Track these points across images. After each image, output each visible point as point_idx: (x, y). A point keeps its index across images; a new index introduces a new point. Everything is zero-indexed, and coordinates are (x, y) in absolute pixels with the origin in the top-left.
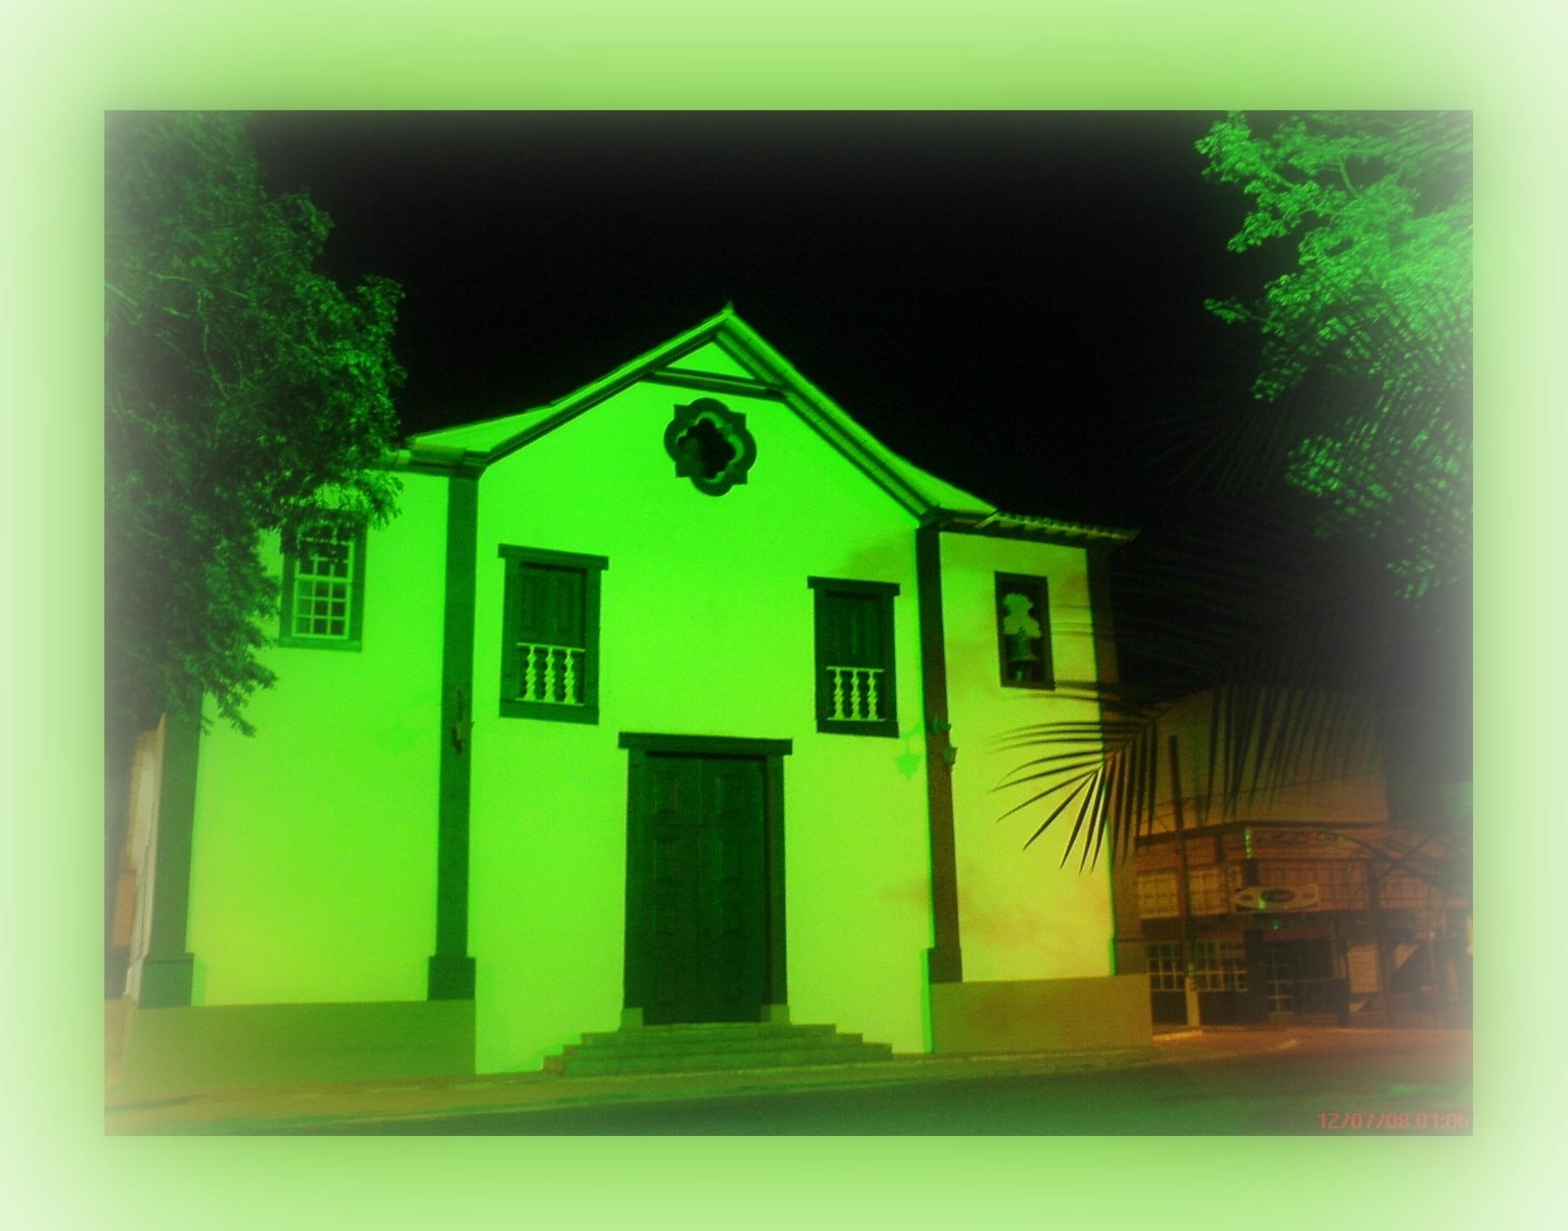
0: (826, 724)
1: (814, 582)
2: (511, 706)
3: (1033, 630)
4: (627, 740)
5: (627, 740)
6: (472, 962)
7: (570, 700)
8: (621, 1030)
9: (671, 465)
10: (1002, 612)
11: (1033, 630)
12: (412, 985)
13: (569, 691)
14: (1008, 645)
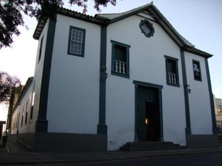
0: (168, 83)
1: (165, 56)
2: (113, 73)
3: (198, 71)
4: (135, 82)
5: (135, 82)
6: (106, 126)
7: (124, 73)
8: (134, 142)
9: (152, 37)
10: (194, 67)
11: (165, 47)
12: (94, 131)
13: (124, 71)
14: (195, 72)
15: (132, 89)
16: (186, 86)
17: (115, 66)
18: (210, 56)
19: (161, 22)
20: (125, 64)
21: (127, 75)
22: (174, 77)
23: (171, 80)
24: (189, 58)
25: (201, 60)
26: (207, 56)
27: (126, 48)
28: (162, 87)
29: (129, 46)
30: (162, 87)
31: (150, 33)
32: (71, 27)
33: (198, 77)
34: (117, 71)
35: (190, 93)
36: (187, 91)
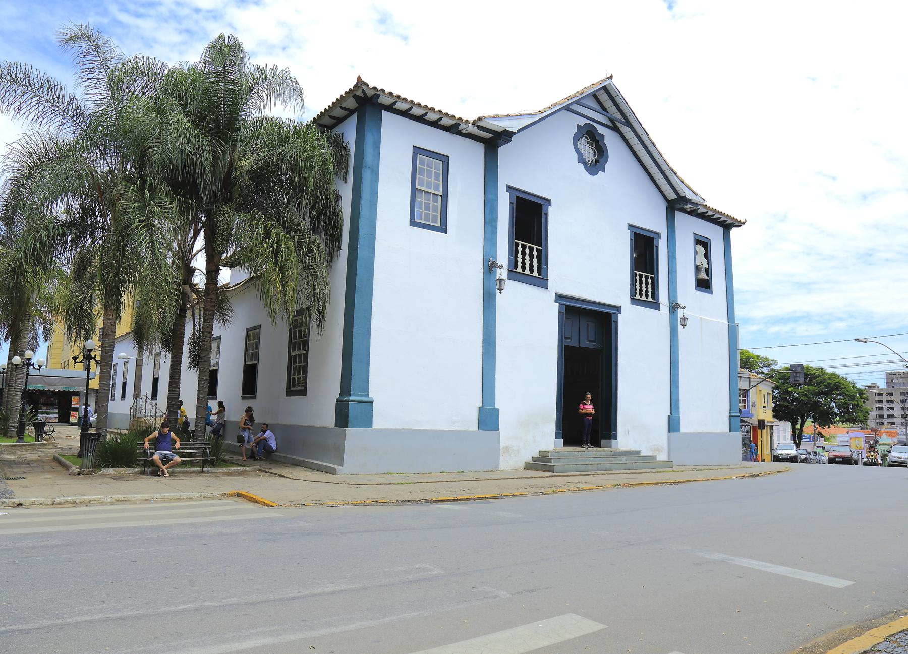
0: (634, 301)
1: (630, 226)
2: (513, 274)
3: (705, 262)
4: (559, 297)
5: (559, 297)
10: (696, 253)
15: (553, 311)
16: (674, 307)
17: (516, 257)
18: (738, 224)
19: (625, 129)
20: (652, 279)
21: (541, 280)
22: (647, 283)
23: (523, 263)
24: (688, 227)
25: (714, 233)
26: (727, 225)
27: (541, 205)
28: (618, 309)
29: (549, 201)
30: (618, 309)
31: (596, 166)
32: (417, 150)
33: (704, 285)
34: (519, 270)
35: (684, 325)
36: (676, 322)
